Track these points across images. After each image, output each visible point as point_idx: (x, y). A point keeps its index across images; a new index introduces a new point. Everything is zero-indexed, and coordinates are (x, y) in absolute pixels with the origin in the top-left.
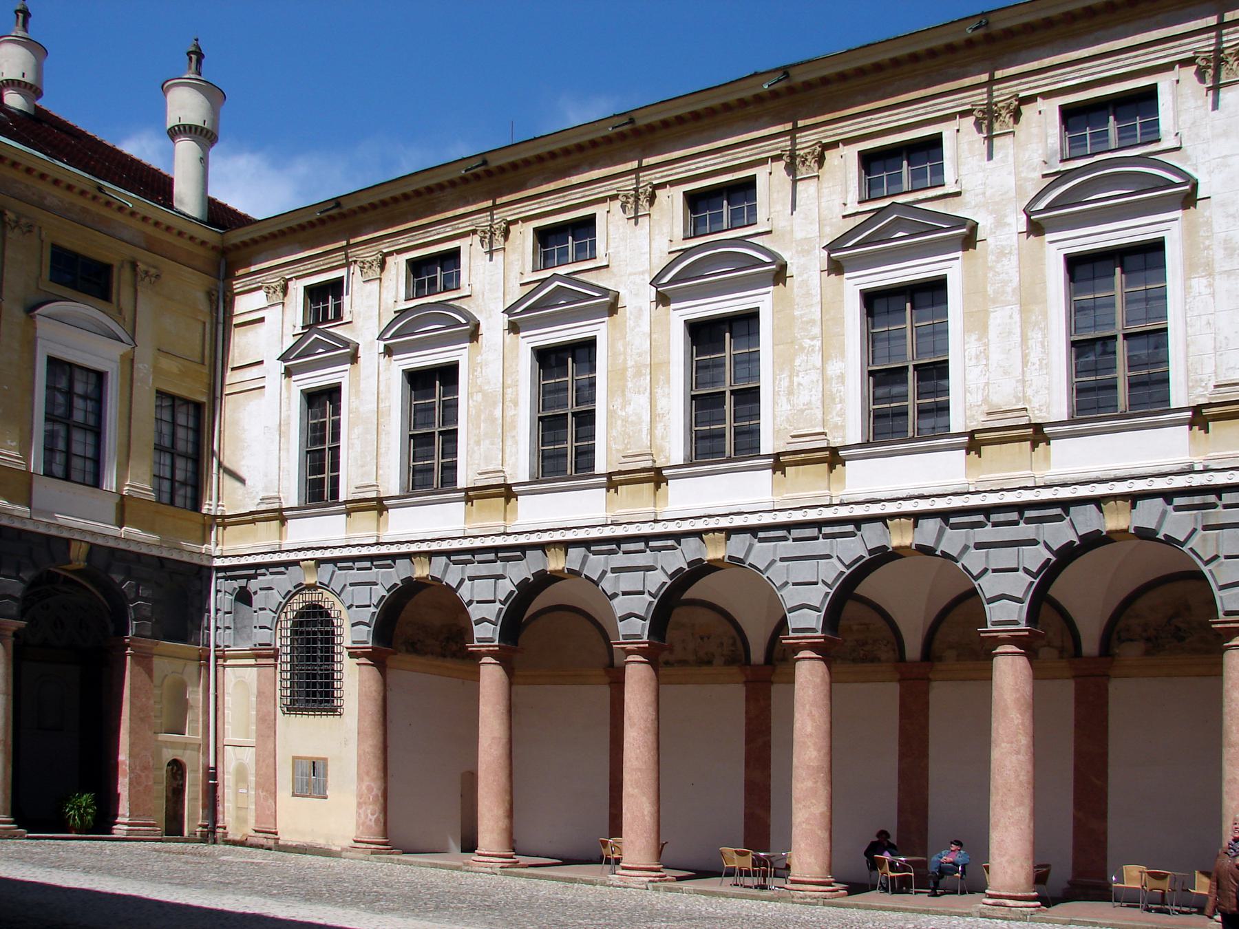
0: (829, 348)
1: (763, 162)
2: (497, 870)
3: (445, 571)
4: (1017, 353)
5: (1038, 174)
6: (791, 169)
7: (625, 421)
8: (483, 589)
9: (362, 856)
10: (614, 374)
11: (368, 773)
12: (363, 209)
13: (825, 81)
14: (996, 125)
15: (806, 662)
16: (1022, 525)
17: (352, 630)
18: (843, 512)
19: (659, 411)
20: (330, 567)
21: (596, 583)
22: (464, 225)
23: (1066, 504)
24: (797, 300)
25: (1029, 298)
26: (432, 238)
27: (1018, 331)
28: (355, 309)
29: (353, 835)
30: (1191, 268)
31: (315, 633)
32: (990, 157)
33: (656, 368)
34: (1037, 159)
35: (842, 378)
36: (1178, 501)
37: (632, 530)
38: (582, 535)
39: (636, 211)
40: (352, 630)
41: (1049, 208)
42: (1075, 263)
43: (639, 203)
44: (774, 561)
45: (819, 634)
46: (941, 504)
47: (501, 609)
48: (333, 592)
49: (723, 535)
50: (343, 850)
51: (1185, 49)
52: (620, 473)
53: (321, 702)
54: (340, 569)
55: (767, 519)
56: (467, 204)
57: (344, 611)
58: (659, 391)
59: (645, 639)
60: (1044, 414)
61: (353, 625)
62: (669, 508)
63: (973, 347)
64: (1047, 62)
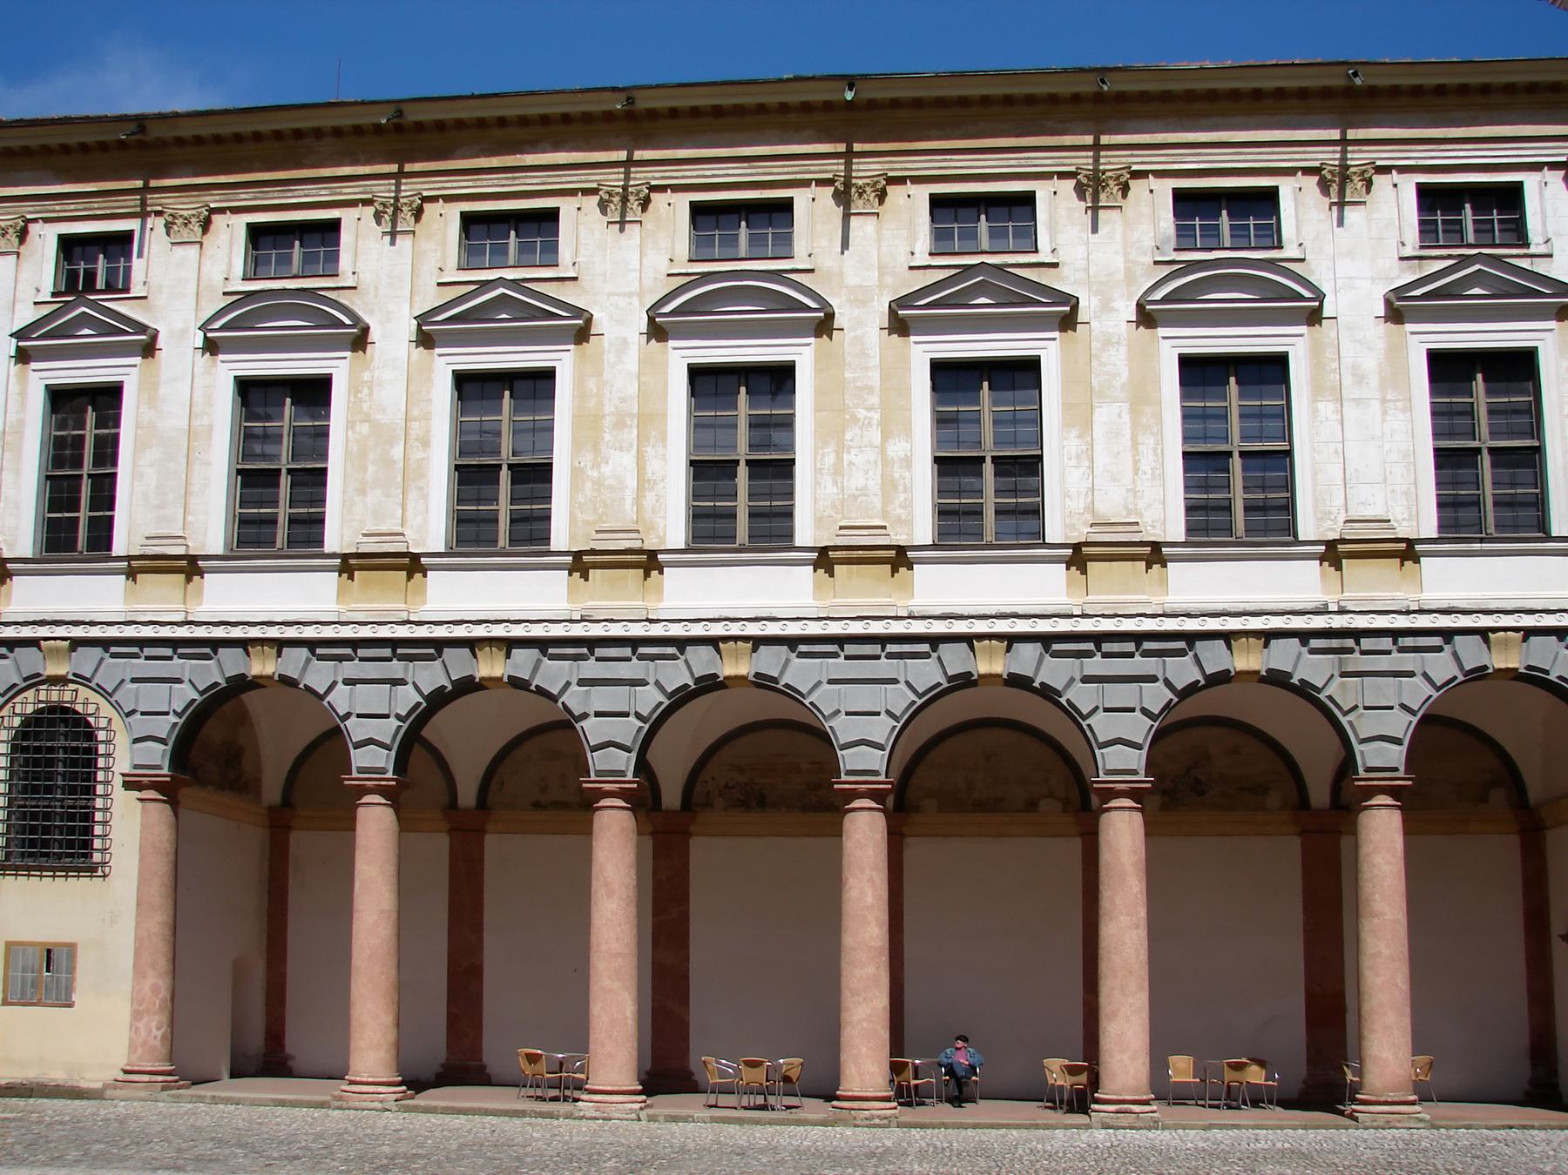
0: (893, 422)
1: (805, 183)
2: (391, 1105)
3: (304, 669)
4: (1127, 458)
5: (1149, 260)
6: (843, 197)
7: (599, 484)
8: (372, 698)
9: (143, 1094)
10: (589, 424)
11: (153, 966)
12: (180, 142)
13: (895, 104)
14: (1103, 196)
15: (865, 813)
16: (1138, 658)
17: (127, 749)
18: (918, 627)
19: (649, 475)
20: (97, 652)
21: (321, 697)
22: (350, 191)
23: (1191, 638)
24: (848, 359)
25: (1141, 397)
26: (299, 200)
27: (1128, 433)
28: (153, 281)
29: (122, 1062)
30: (1318, 390)
31: (51, 750)
32: (1095, 230)
33: (649, 420)
34: (1149, 243)
35: (907, 462)
36: (1315, 643)
37: (616, 630)
38: (537, 631)
39: (623, 215)
40: (127, 749)
41: (1164, 300)
42: (462, 380)
43: (624, 207)
44: (819, 683)
45: (390, 775)
46: (1044, 626)
47: (400, 727)
48: (100, 690)
49: (750, 645)
50: (106, 1086)
51: (1071, 161)
52: (593, 552)
53: (59, 856)
54: (114, 656)
55: (814, 629)
56: (355, 162)
57: (117, 723)
58: (649, 449)
59: (630, 776)
60: (1158, 532)
61: (136, 741)
62: (204, 607)
63: (1074, 444)
64: (495, 162)
